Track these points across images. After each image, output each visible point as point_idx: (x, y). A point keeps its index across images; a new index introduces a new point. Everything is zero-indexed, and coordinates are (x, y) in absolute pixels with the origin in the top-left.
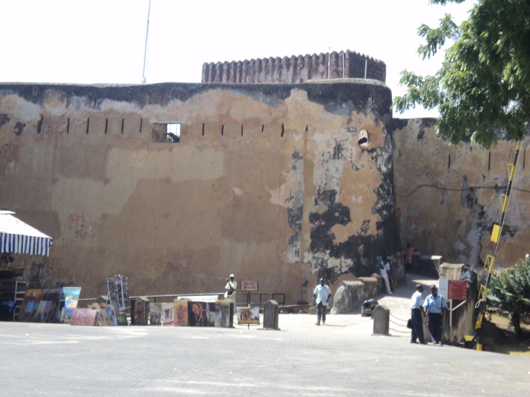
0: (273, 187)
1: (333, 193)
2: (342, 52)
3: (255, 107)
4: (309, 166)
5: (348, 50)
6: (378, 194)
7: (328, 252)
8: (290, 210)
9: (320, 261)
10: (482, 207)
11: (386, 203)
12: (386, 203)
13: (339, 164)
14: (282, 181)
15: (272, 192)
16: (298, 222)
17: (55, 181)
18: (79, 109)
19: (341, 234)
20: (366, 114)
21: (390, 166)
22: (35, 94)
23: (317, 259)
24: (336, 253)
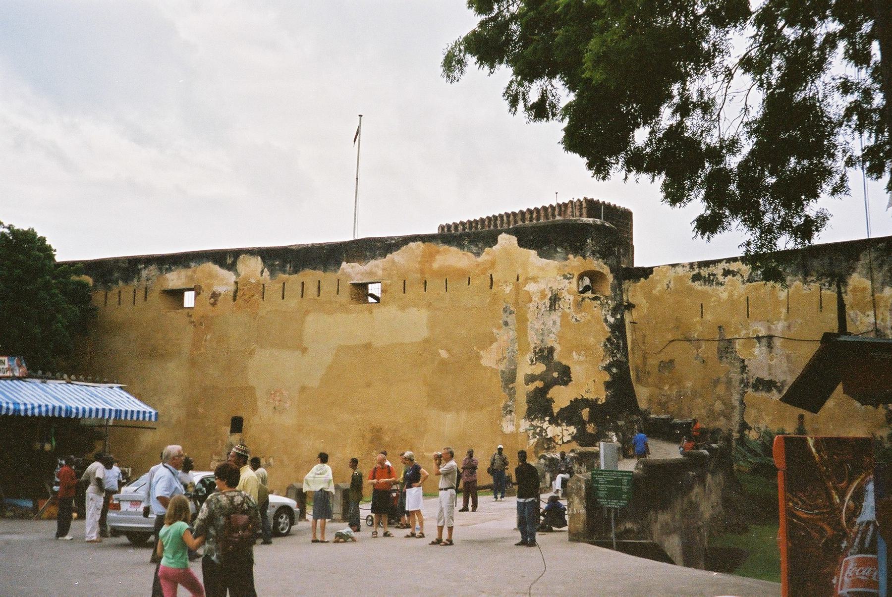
0: (484, 348)
1: (551, 350)
2: (579, 200)
3: (455, 258)
4: (522, 321)
5: (585, 198)
7: (547, 419)
8: (503, 372)
9: (538, 430)
10: (743, 361)
11: (615, 359)
12: (615, 359)
13: (556, 316)
14: (492, 340)
15: (482, 353)
16: (511, 386)
17: (251, 353)
19: (561, 397)
20: (584, 257)
21: (619, 317)
22: (229, 261)
23: (535, 427)
24: (554, 421)
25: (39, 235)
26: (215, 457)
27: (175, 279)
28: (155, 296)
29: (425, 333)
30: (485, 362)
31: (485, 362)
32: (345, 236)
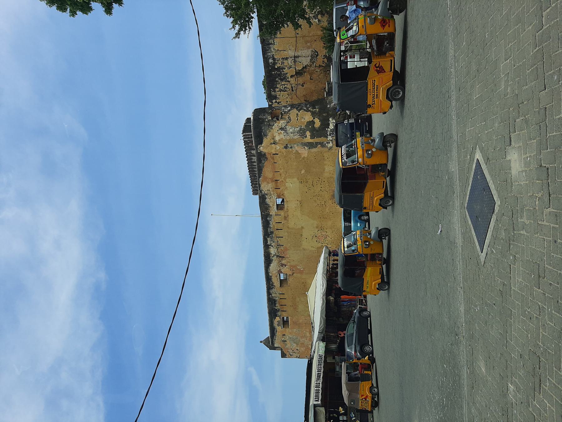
6: (300, 110)
13: (288, 128)
15: (302, 156)
17: (304, 249)
18: (274, 267)
19: (318, 123)
25: (54, 7)
26: (334, 287)
27: (276, 283)
28: (283, 290)
29: (295, 179)
30: (306, 155)
31: (306, 155)
32: (268, 328)
